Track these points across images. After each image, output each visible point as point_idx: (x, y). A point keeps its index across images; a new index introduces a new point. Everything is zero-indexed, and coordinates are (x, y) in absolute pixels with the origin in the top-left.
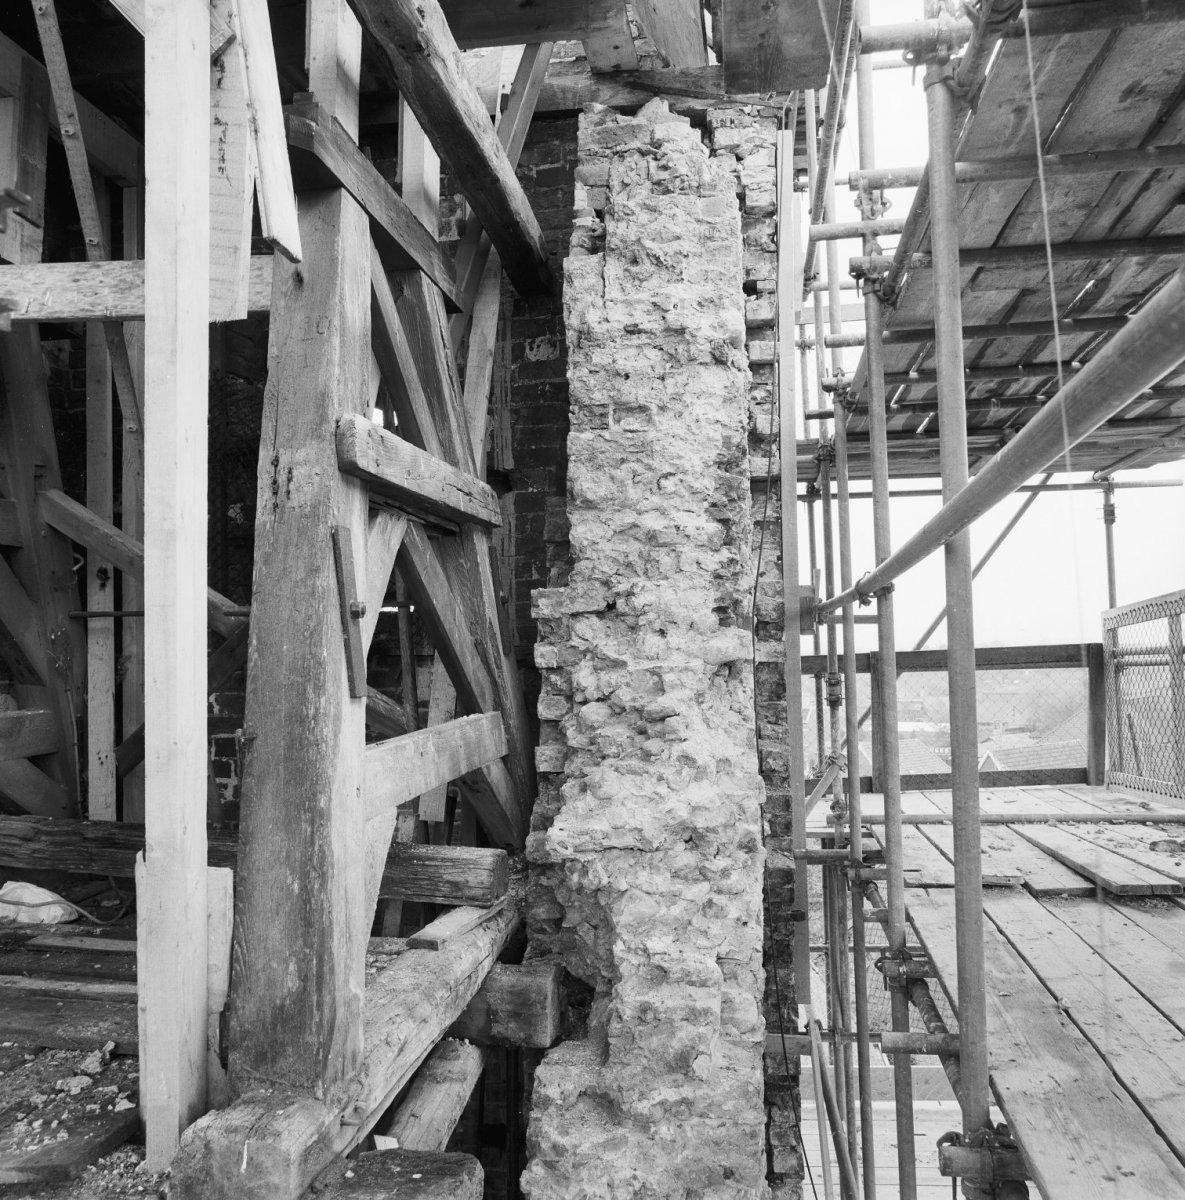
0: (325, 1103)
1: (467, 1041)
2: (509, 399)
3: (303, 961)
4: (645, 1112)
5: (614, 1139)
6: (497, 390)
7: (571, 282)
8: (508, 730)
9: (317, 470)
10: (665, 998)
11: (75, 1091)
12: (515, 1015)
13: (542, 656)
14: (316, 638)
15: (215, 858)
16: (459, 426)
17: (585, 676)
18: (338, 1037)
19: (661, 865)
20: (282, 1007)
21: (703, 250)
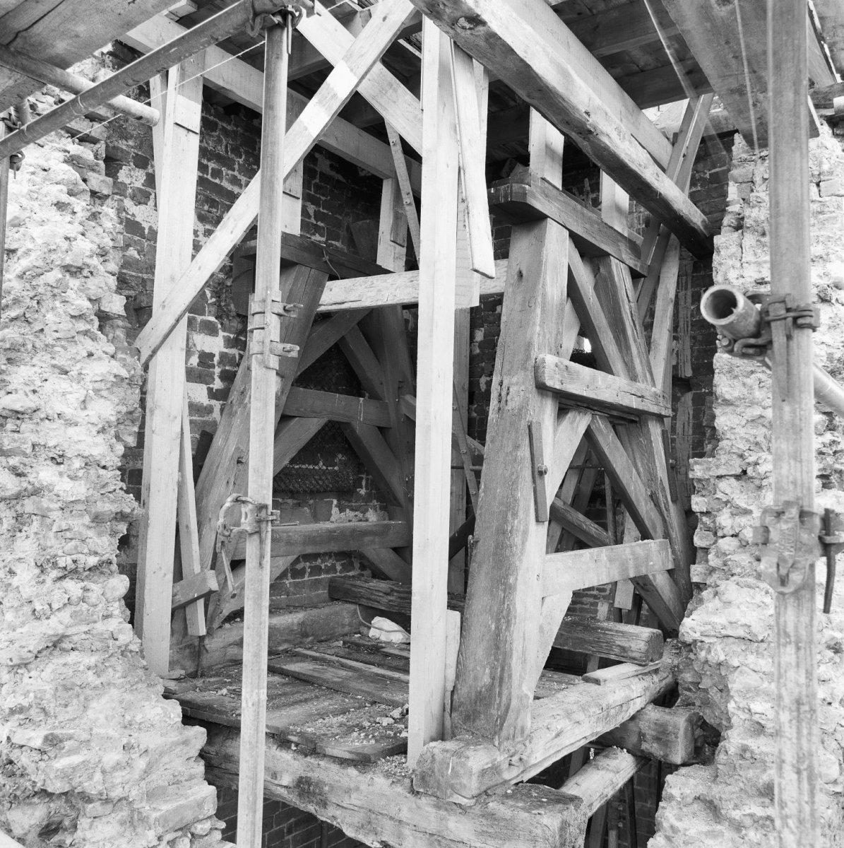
0: (499, 750)
1: (625, 750)
2: (689, 329)
3: (493, 668)
4: (737, 818)
5: (713, 831)
6: (682, 302)
7: (719, 252)
8: (674, 552)
9: (523, 388)
10: (759, 745)
11: (385, 724)
12: (657, 739)
13: (697, 503)
14: (515, 486)
15: (451, 606)
16: (639, 352)
17: (724, 519)
18: (511, 715)
19: (765, 652)
20: (481, 691)
21: (816, 221)
